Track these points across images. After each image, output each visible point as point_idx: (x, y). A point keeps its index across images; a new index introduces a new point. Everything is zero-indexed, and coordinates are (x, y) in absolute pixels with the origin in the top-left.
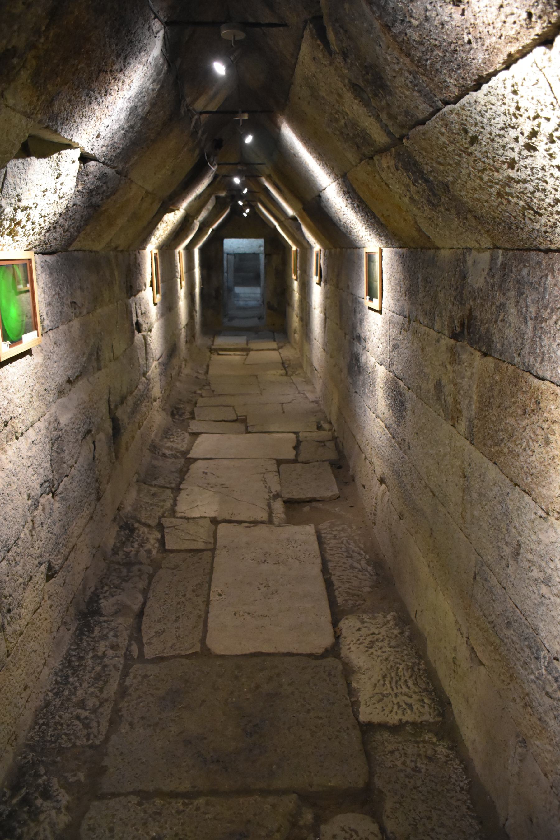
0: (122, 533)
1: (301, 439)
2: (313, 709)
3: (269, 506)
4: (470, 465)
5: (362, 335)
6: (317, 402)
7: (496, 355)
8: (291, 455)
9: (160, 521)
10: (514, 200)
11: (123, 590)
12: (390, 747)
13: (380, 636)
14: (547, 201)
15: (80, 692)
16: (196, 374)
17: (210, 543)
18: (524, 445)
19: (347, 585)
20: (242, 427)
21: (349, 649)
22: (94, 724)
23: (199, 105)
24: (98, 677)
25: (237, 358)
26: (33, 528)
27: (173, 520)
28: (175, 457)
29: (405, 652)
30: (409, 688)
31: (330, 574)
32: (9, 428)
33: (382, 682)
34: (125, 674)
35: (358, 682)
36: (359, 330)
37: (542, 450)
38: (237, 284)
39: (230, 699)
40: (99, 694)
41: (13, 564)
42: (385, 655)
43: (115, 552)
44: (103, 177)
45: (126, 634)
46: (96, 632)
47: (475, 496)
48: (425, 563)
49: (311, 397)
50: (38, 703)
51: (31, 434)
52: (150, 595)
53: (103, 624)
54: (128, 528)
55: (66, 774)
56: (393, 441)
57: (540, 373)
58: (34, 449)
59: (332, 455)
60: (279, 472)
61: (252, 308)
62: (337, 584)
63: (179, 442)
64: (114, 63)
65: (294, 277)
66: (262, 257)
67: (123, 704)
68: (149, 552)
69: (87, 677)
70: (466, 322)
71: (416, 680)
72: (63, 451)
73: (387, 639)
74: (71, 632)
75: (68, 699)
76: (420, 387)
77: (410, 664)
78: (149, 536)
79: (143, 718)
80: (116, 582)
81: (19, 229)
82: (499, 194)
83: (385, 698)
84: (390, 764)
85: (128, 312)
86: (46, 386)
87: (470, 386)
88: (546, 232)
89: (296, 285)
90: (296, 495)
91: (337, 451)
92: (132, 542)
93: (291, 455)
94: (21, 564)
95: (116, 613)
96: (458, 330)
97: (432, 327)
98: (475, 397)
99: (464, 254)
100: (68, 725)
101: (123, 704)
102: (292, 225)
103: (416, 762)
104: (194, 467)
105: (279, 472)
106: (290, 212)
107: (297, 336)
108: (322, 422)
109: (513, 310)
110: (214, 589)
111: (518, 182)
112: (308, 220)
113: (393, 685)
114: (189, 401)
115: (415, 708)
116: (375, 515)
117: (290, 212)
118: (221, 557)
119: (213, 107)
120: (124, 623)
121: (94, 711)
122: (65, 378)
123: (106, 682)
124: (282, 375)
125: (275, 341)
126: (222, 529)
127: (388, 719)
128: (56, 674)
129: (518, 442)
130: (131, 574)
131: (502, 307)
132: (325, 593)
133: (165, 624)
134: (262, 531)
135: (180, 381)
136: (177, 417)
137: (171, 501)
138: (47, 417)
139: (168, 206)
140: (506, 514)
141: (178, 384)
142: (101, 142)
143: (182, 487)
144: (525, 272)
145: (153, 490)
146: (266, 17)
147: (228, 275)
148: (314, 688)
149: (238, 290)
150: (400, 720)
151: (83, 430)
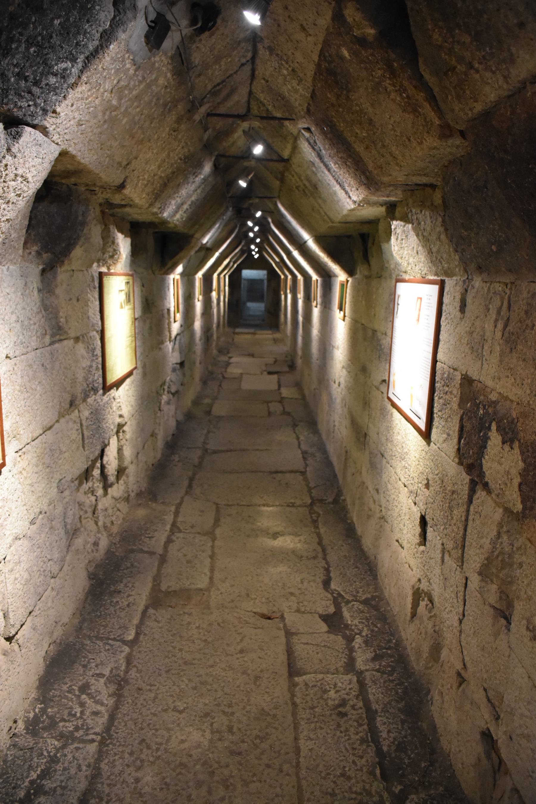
147: (244, 293)
149: (250, 305)
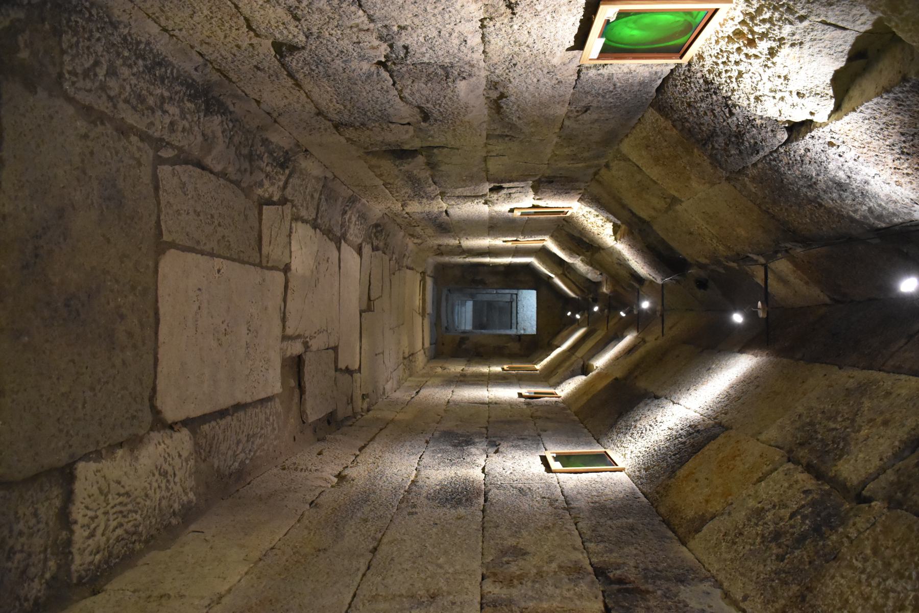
1: (355, 375)
2: (95, 395)
3: (299, 336)
8: (342, 365)
12: (42, 511)
13: (172, 483)
15: (125, 72)
17: (268, 262)
19: (221, 437)
20: (364, 307)
21: (159, 443)
22: (89, 85)
24: (141, 99)
27: (289, 218)
28: (342, 226)
29: (154, 521)
30: (114, 530)
31: (232, 415)
33: (122, 491)
34: (144, 137)
35: (122, 457)
38: (475, 305)
39: (109, 278)
40: (122, 97)
42: (151, 493)
43: (265, 142)
45: (184, 143)
46: (189, 105)
48: (274, 543)
49: (388, 386)
50: (116, 12)
52: (222, 181)
55: (27, 32)
59: (340, 415)
62: (223, 422)
65: (505, 367)
67: (109, 129)
68: (261, 185)
69: (142, 84)
70: (628, 586)
71: (122, 539)
73: (169, 494)
74: (193, 72)
75: (118, 54)
77: (140, 529)
79: (92, 153)
80: (236, 139)
83: (103, 497)
84: (20, 512)
85: (523, 178)
89: (497, 369)
90: (308, 369)
91: (349, 419)
93: (342, 365)
100: (88, 48)
101: (109, 129)
103: (22, 551)
104: (332, 246)
106: (600, 362)
108: (368, 400)
113: (118, 508)
115: (90, 541)
116: (296, 469)
118: (253, 274)
120: (192, 143)
121: (103, 88)
123: (134, 108)
126: (279, 277)
127: (78, 503)
128: (148, 43)
134: (277, 331)
137: (306, 217)
139: (631, 226)
143: (318, 230)
145: (316, 196)
148: (119, 396)
149: (470, 304)
150: (76, 522)
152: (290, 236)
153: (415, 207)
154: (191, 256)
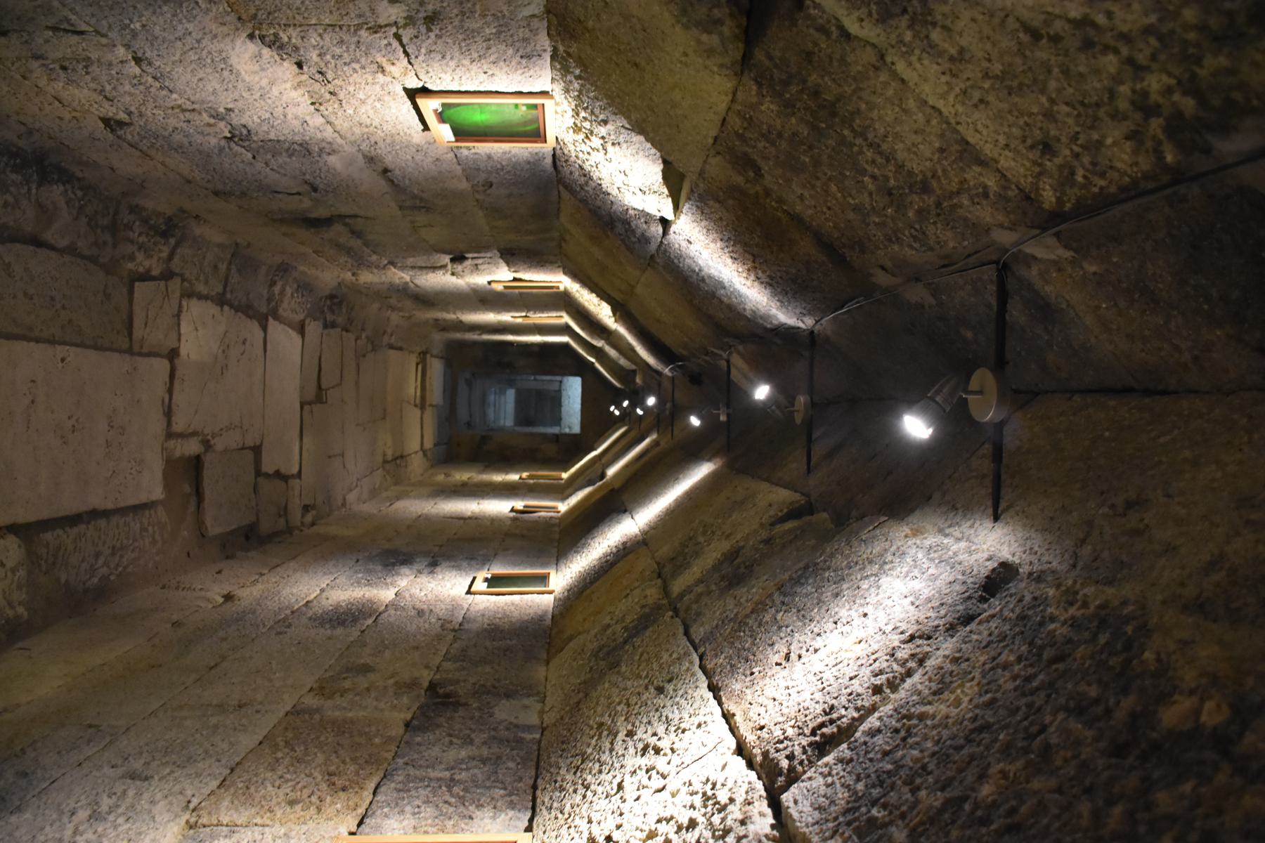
0: (161, 220)
3: (194, 434)
4: (257, 712)
5: (438, 569)
6: (344, 505)
7: (406, 737)
8: (268, 467)
9: (177, 274)
10: (593, 742)
11: (76, 219)
14: (589, 777)
16: (389, 331)
18: (288, 776)
23: (737, 360)
25: (412, 391)
26: (184, 110)
27: (178, 294)
28: (269, 300)
31: (89, 523)
32: (328, 96)
36: (444, 564)
37: (282, 797)
38: (519, 394)
41: (135, 81)
43: (135, 209)
44: (645, 239)
46: (14, 176)
47: (213, 720)
49: (351, 497)
51: (318, 121)
52: (67, 258)
53: (26, 188)
54: (169, 228)
56: (288, 612)
57: (382, 789)
58: (296, 123)
59: (265, 526)
60: (243, 449)
61: (484, 414)
62: (74, 532)
63: (291, 305)
64: (764, 272)
65: (525, 475)
66: (555, 430)
68: (132, 258)
72: (290, 156)
76: (364, 645)
78: (155, 258)
81: (582, 136)
82: (601, 725)
85: (480, 248)
86: (381, 144)
87: (366, 707)
88: (556, 782)
89: (514, 477)
92: (147, 234)
93: (268, 467)
94: (132, 90)
95: (40, 206)
96: (441, 691)
97: (446, 658)
98: (350, 715)
99: (538, 693)
102: (594, 473)
104: (255, 327)
105: (243, 449)
106: (611, 472)
107: (440, 478)
108: (314, 512)
109: (463, 753)
110: (72, 353)
111: (612, 744)
112: (598, 496)
114: (350, 321)
116: (177, 588)
117: (611, 472)
119: (735, 375)
122: (391, 167)
124: (385, 455)
125: (435, 445)
126: (162, 365)
129: (291, 769)
130: (99, 231)
131: (468, 741)
132: (61, 514)
133: (21, 279)
134: (156, 425)
135: (380, 309)
136: (328, 302)
138: (339, 141)
139: (620, 310)
140: (190, 760)
141: (376, 306)
142: (684, 244)
144: (511, 764)
145: (223, 267)
146: (818, 450)
147: (532, 381)
149: (511, 394)
151: (318, 181)
152: (178, 315)
153: (366, 277)
154: (21, 346)
